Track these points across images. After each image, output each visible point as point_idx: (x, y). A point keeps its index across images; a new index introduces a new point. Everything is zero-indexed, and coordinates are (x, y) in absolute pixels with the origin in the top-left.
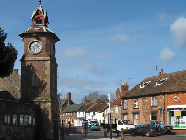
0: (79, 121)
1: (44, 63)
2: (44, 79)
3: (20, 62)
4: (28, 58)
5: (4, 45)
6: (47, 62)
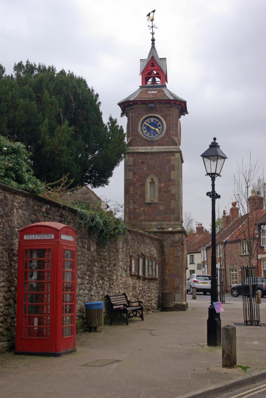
0: (143, 238)
4: (138, 148)
6: (174, 156)
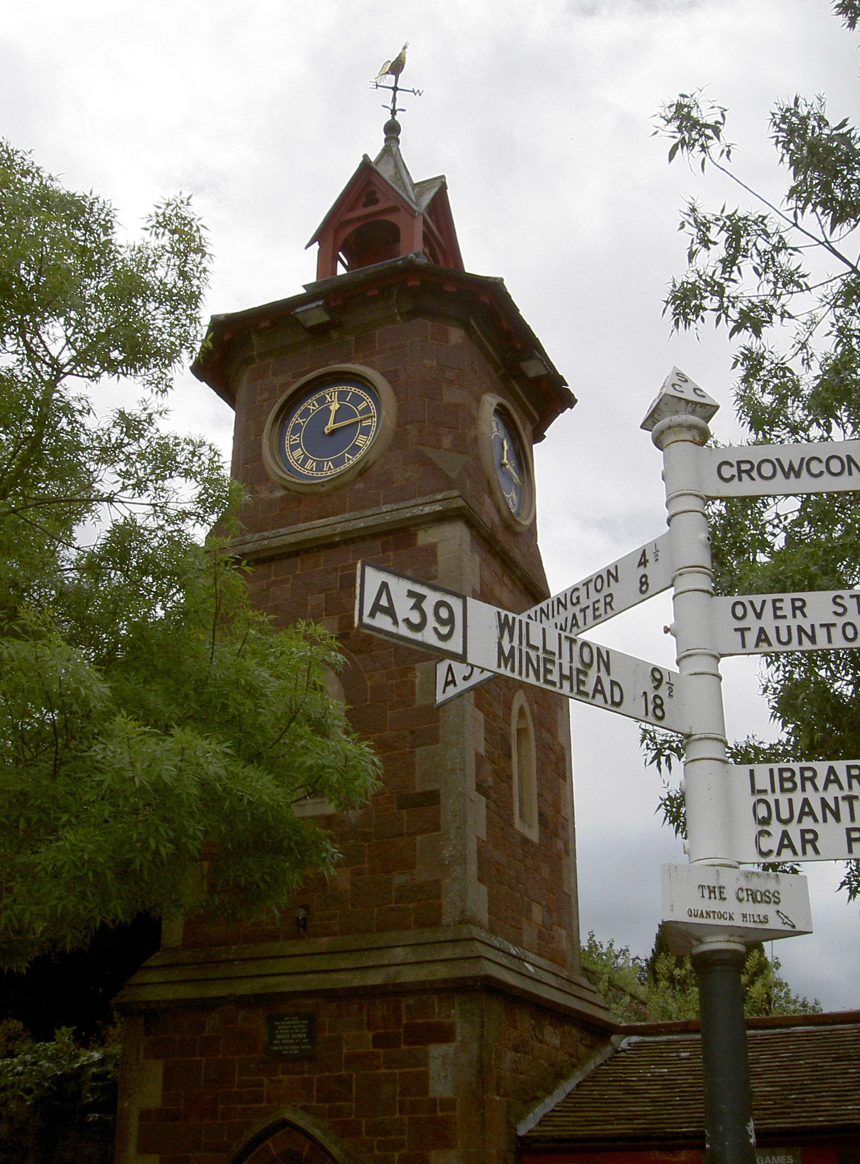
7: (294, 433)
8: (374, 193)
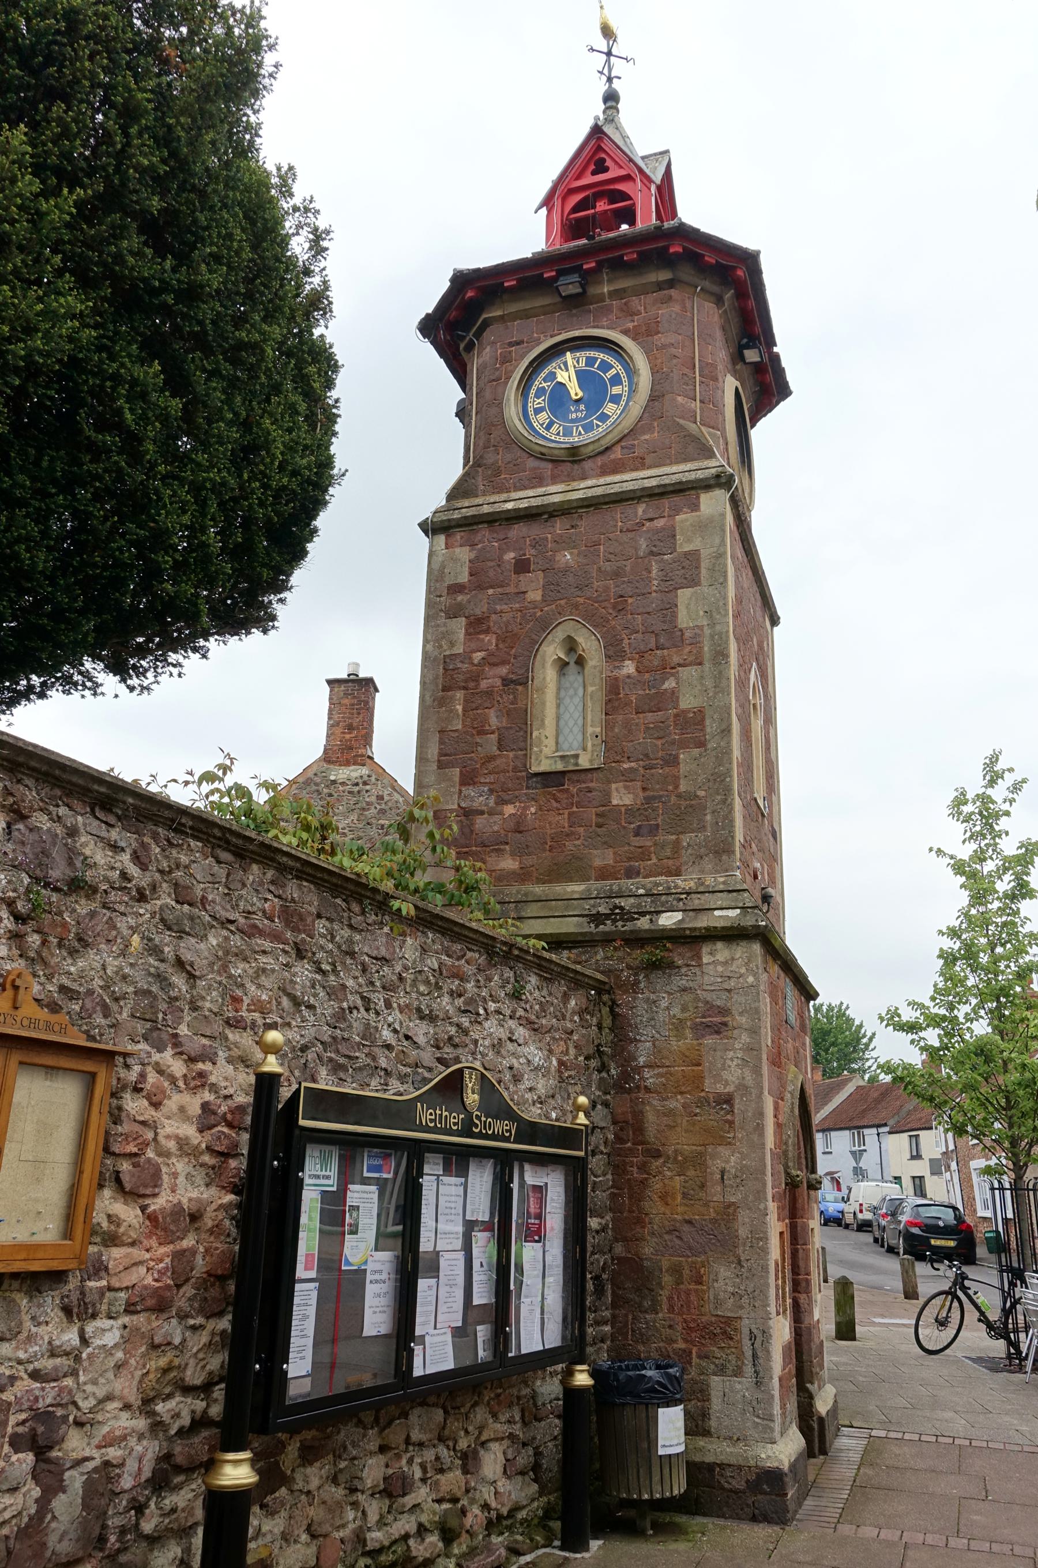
1: (660, 523)
2: (670, 684)
3: (424, 541)
4: (504, 496)
5: (245, 151)
6: (695, 507)
7: (537, 396)
8: (604, 160)
